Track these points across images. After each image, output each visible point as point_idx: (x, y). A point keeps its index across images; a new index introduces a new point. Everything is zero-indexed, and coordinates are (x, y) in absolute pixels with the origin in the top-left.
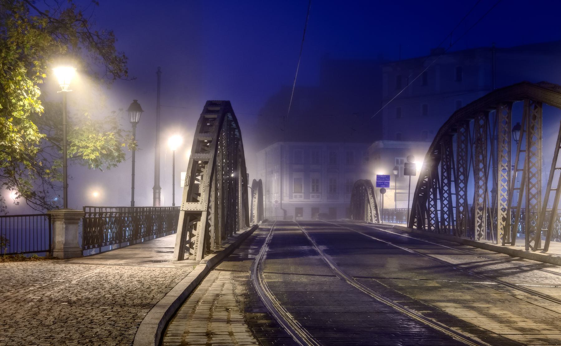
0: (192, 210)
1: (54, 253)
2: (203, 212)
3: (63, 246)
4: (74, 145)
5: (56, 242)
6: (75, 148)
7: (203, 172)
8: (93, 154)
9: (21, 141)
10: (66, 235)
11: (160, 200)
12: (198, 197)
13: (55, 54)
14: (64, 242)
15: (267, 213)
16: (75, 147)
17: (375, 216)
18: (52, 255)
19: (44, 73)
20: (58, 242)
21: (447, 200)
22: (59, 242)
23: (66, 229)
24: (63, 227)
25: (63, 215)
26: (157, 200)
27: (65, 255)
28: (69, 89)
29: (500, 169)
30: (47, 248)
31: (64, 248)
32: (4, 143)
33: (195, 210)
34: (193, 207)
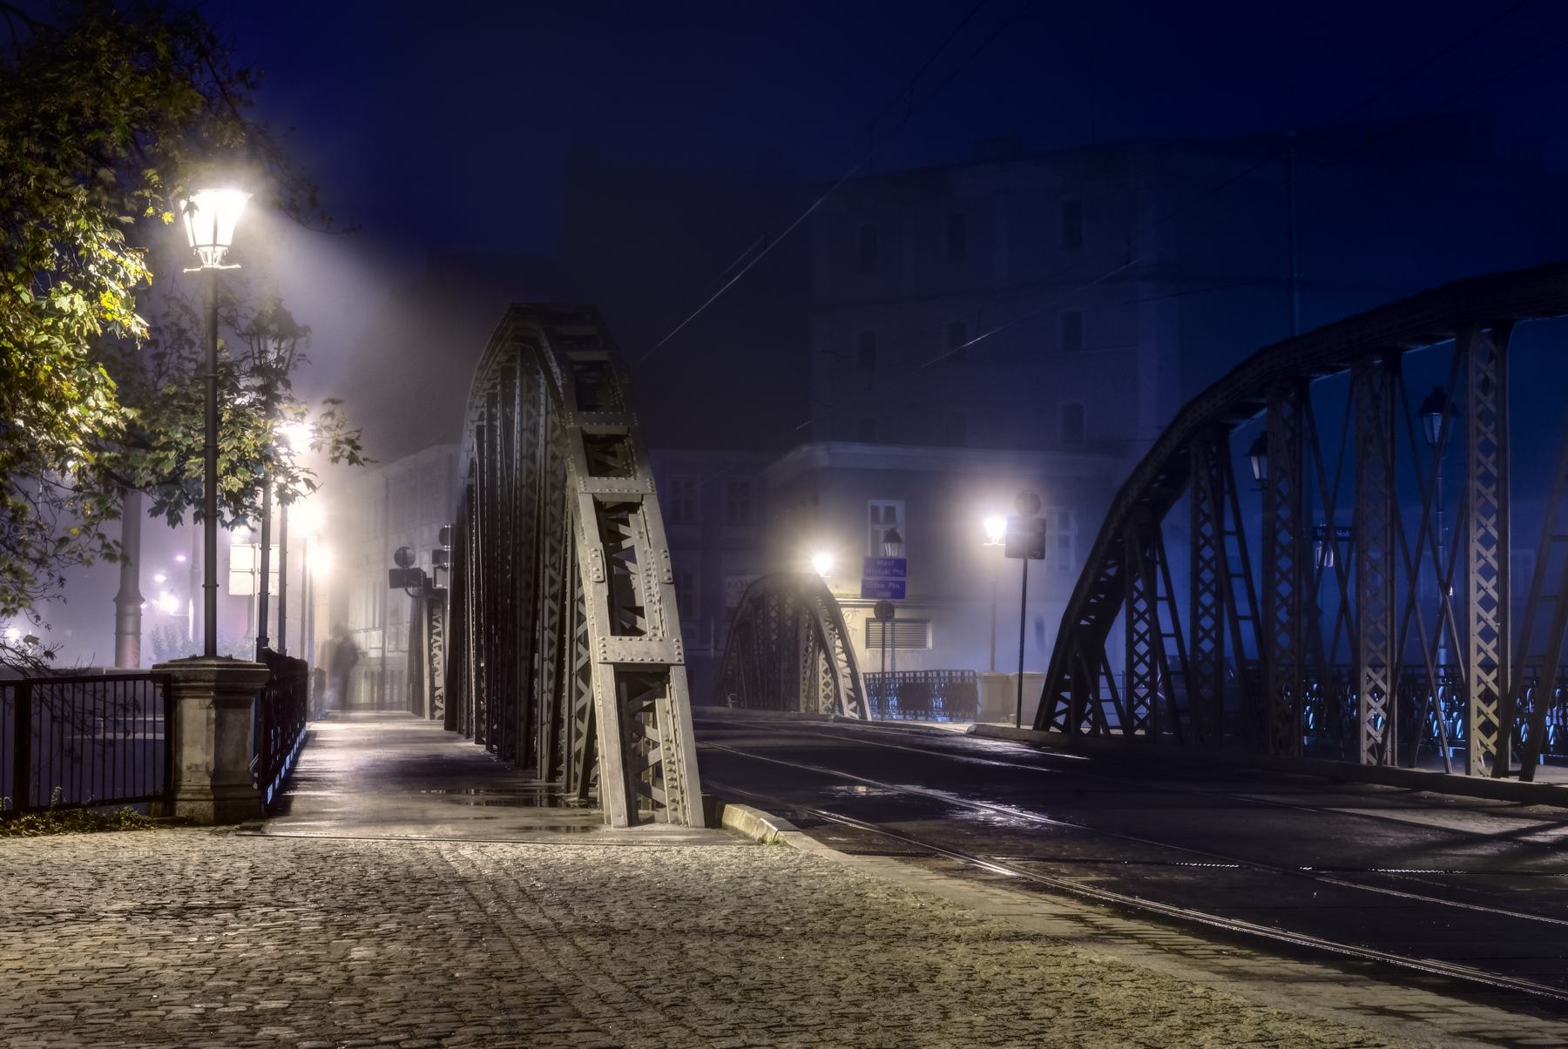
0: (637, 660)
1: (179, 804)
2: (672, 668)
3: (207, 782)
4: (166, 447)
5: (184, 768)
6: (172, 454)
7: (628, 537)
8: (234, 474)
9: (90, 431)
10: (217, 746)
11: (138, 641)
12: (638, 618)
13: (204, 149)
14: (212, 768)
15: (388, 691)
16: (171, 450)
17: (848, 695)
18: (172, 811)
19: (166, 209)
20: (189, 768)
21: (1146, 641)
22: (194, 768)
23: (220, 724)
24: (208, 718)
25: (213, 677)
26: (130, 639)
27: (217, 809)
28: (227, 259)
29: (1475, 534)
30: (160, 790)
31: (212, 786)
32: (48, 438)
33: (647, 660)
34: (631, 650)
